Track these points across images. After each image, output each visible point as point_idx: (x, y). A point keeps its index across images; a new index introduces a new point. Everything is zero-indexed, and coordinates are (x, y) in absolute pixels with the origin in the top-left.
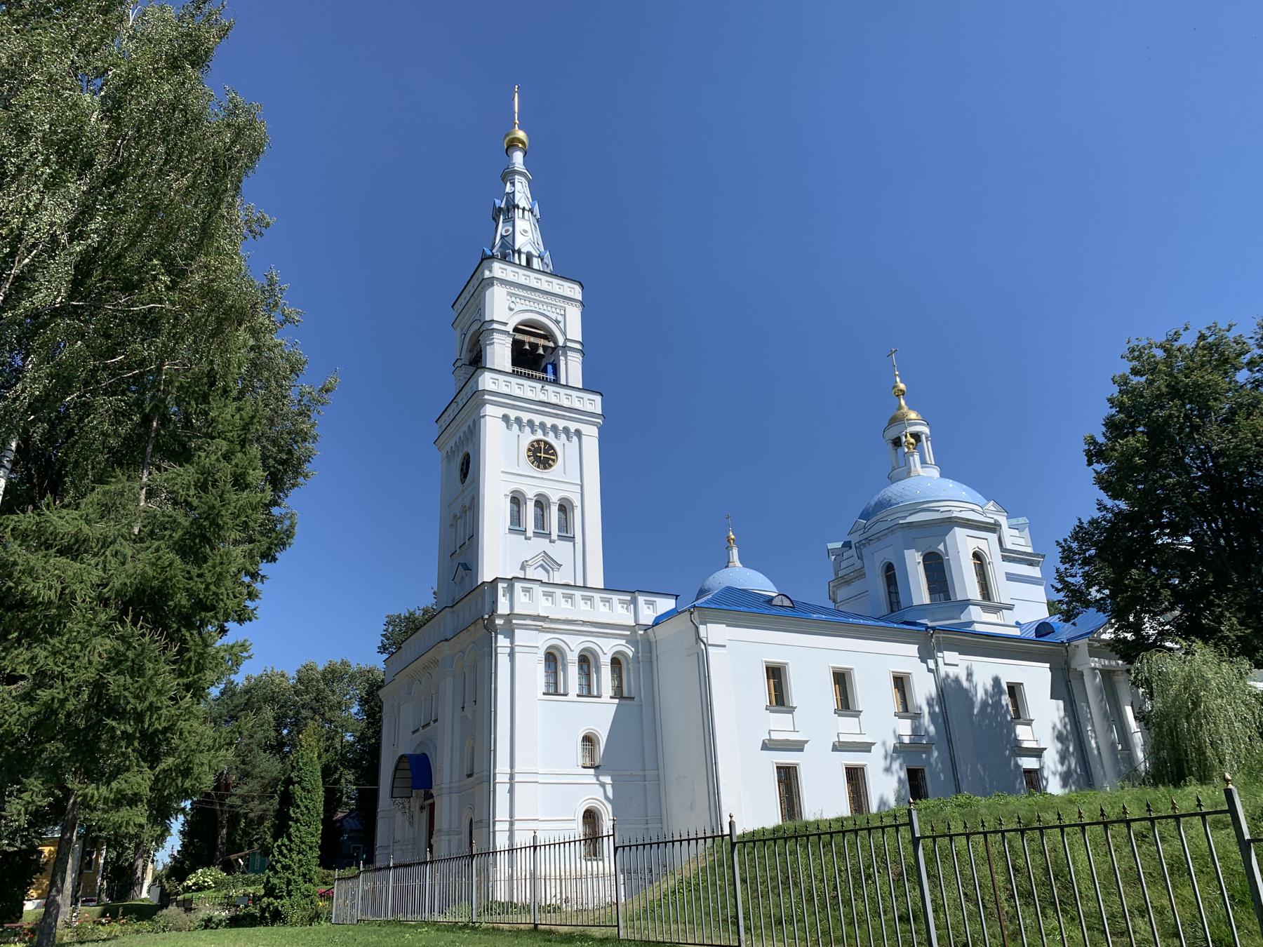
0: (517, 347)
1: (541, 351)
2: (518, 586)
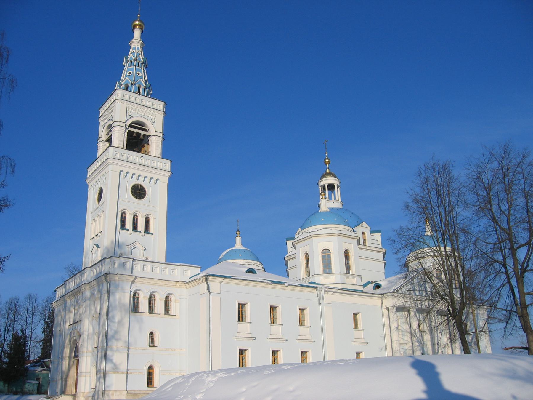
1: (141, 137)
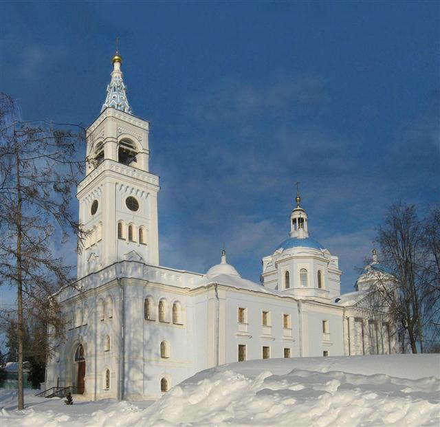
1: (130, 154)
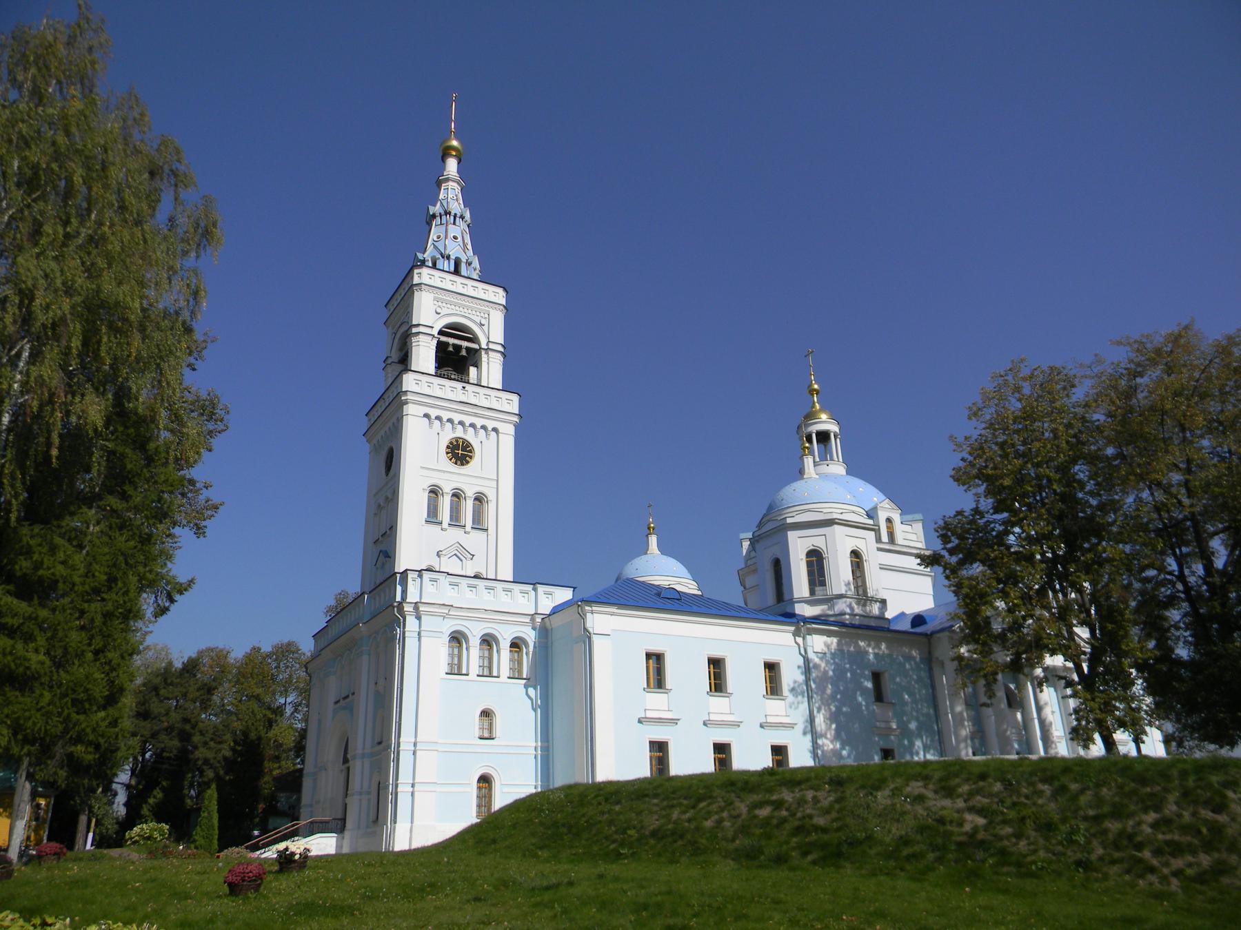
0: (441, 347)
1: (464, 353)
2: (426, 575)
